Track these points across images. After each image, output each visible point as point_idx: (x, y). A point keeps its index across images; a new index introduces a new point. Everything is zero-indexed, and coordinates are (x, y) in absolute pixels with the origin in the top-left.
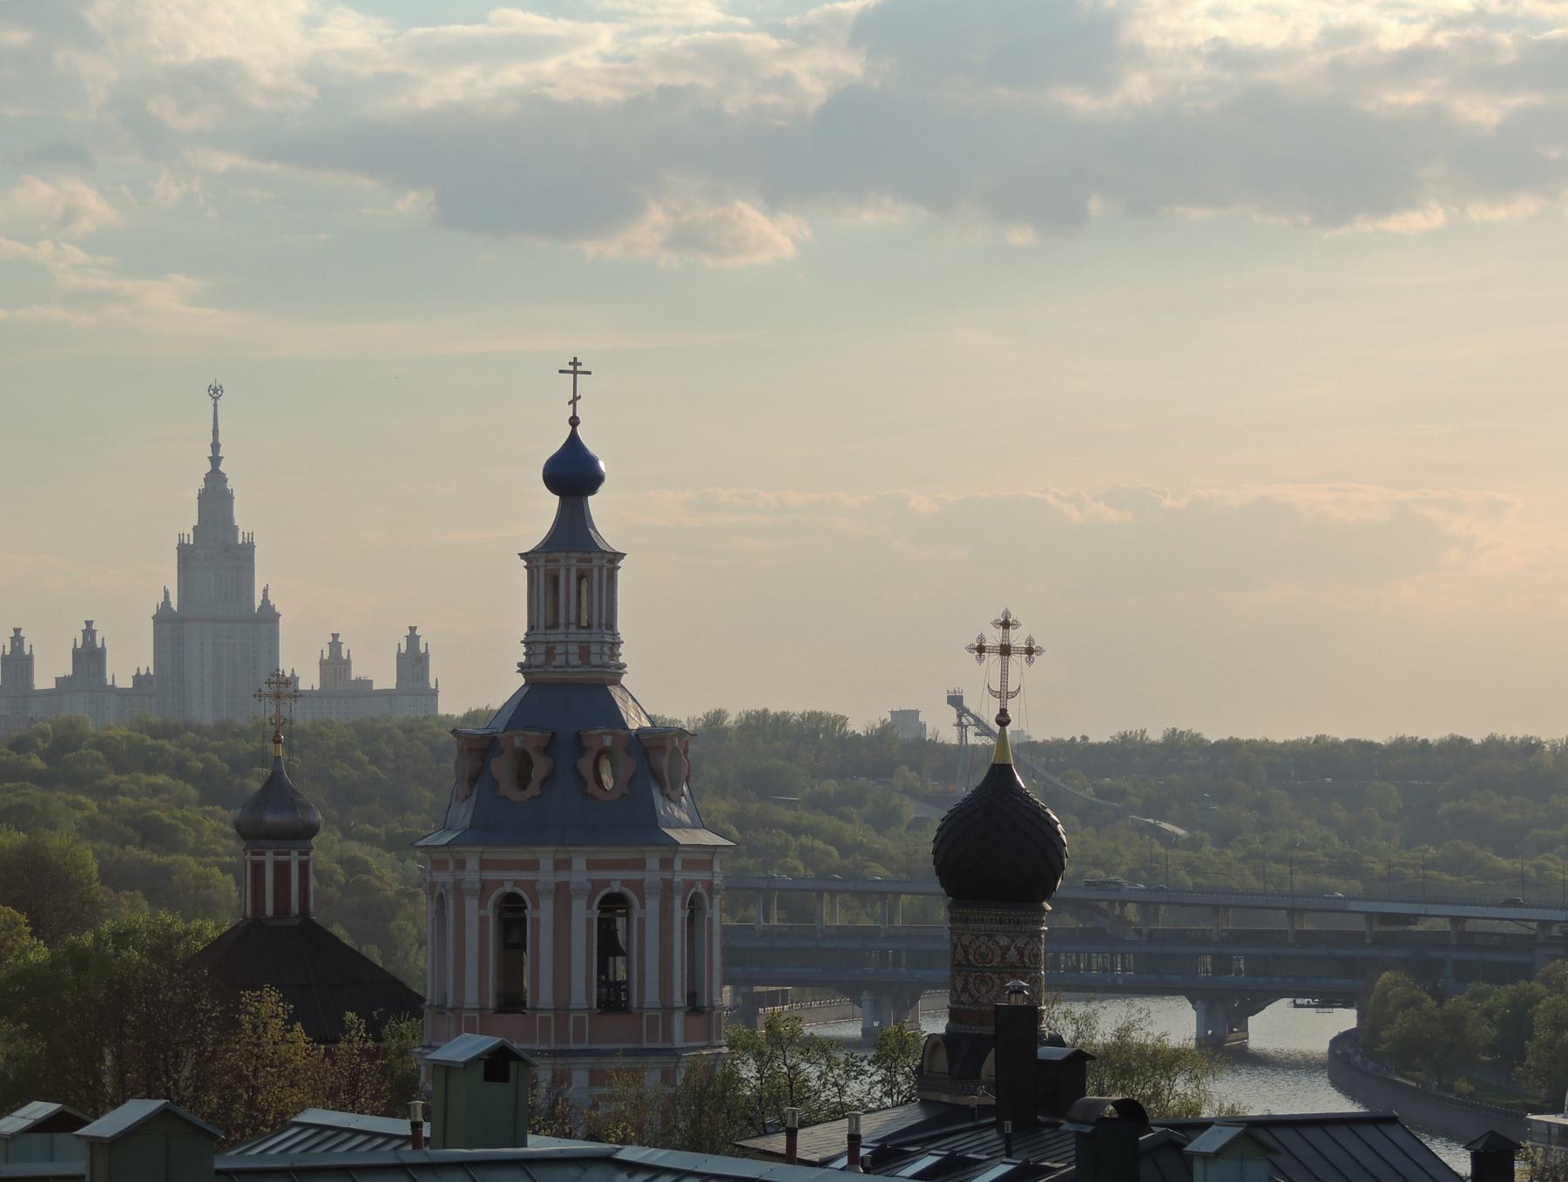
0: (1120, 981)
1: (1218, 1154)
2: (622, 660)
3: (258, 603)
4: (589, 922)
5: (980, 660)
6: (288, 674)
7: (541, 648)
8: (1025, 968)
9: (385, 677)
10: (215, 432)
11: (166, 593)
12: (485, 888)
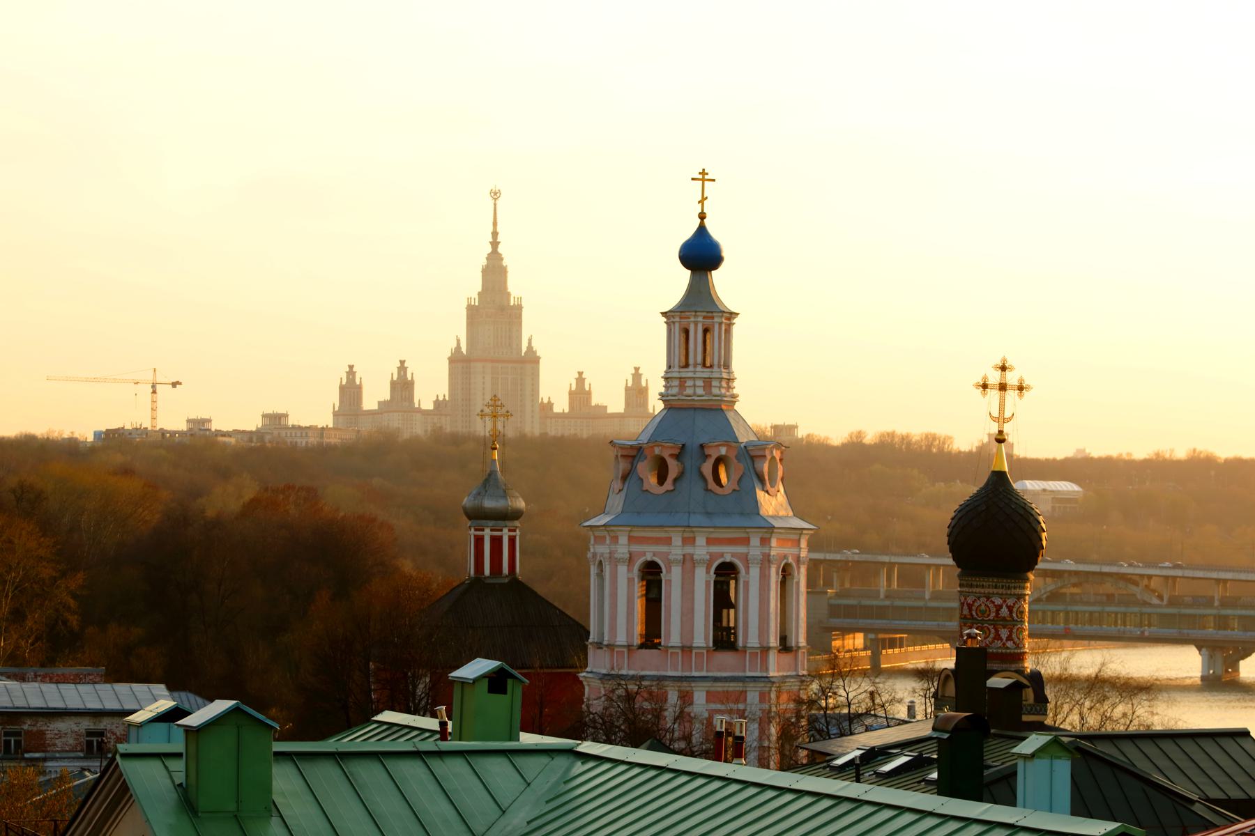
0: (1146, 634)
1: (1033, 756)
2: (735, 391)
3: (524, 349)
4: (707, 583)
5: (984, 394)
6: (546, 401)
7: (676, 383)
8: (1012, 622)
9: (616, 404)
10: (495, 224)
11: (458, 341)
12: (631, 560)
